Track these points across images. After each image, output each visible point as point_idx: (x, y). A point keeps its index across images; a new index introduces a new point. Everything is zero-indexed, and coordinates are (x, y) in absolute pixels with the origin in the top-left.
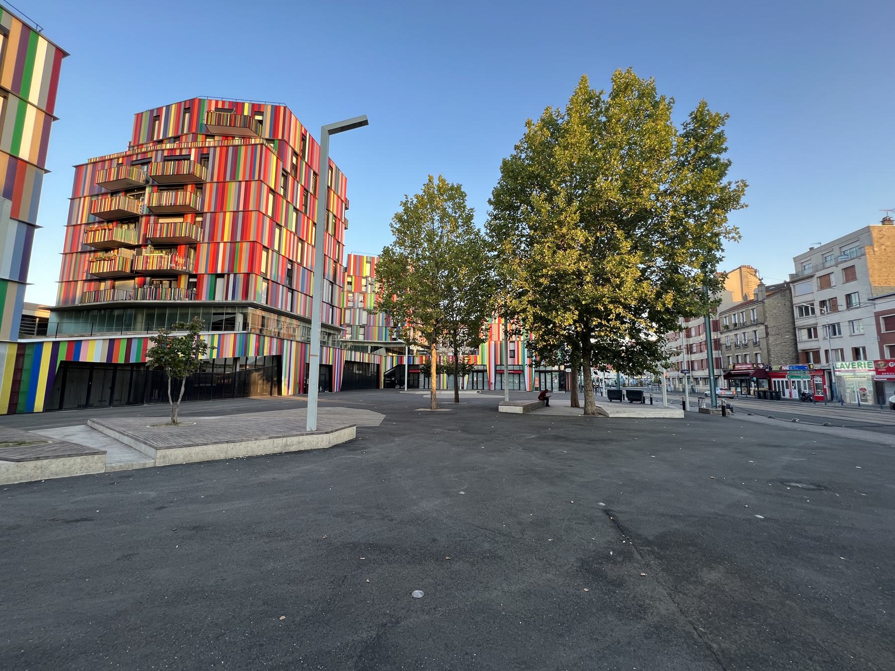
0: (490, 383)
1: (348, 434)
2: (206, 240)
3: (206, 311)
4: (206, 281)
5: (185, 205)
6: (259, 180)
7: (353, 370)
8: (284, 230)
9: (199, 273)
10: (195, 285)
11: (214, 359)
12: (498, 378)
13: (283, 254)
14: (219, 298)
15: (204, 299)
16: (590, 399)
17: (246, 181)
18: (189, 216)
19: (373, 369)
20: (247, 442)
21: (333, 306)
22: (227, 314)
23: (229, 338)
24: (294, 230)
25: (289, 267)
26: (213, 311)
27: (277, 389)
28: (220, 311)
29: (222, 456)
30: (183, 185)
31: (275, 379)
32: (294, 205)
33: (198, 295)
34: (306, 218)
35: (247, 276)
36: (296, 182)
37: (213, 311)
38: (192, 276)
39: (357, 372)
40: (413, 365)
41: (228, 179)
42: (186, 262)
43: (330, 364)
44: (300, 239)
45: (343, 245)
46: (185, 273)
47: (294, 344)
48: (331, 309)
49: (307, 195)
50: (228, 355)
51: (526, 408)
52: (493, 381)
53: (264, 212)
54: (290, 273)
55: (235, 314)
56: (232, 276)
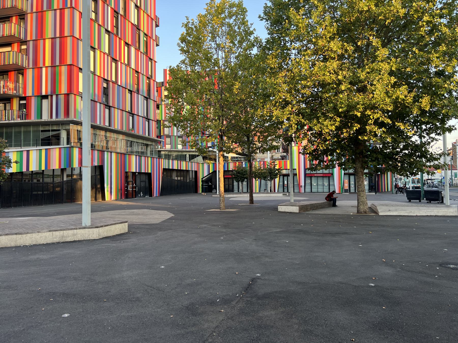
0: (300, 187)
1: (122, 228)
2: (31, 66)
3: (35, 129)
4: (34, 102)
5: (11, 36)
6: (71, 7)
7: (171, 176)
8: (98, 52)
9: (27, 95)
10: (25, 106)
11: (43, 171)
12: (308, 181)
13: (99, 75)
14: (45, 118)
15: (33, 118)
16: (362, 199)
17: (60, 9)
18: (16, 45)
19: (192, 175)
20: (31, 234)
21: (148, 120)
22: (53, 131)
23: (55, 151)
24: (107, 51)
25: (105, 85)
26: (41, 129)
27: (101, 195)
28: (47, 128)
29: (13, 244)
30: (9, 17)
31: (99, 186)
32: (106, 27)
33: (27, 116)
34: (118, 39)
35: (67, 96)
36: (106, 5)
37: (41, 129)
38: (22, 98)
39: (176, 178)
40: (228, 171)
41: (45, 9)
42: (16, 87)
43: (149, 172)
44: (113, 59)
45: (156, 62)
46: (16, 97)
47: (114, 155)
48: (147, 123)
49: (118, 16)
50: (55, 167)
51: (303, 208)
52: (302, 184)
53: (78, 37)
54: (106, 92)
55: (59, 130)
56: (54, 97)
